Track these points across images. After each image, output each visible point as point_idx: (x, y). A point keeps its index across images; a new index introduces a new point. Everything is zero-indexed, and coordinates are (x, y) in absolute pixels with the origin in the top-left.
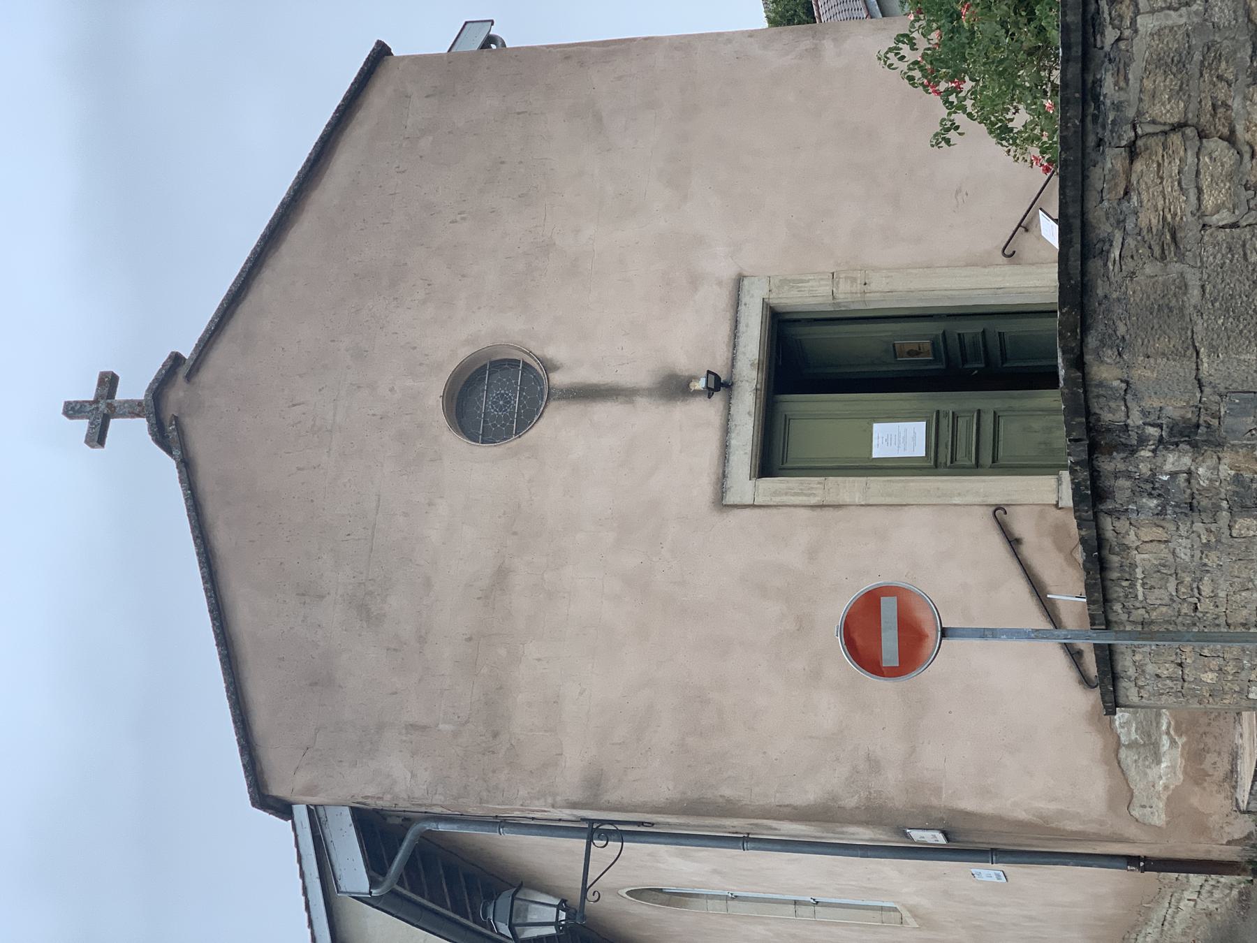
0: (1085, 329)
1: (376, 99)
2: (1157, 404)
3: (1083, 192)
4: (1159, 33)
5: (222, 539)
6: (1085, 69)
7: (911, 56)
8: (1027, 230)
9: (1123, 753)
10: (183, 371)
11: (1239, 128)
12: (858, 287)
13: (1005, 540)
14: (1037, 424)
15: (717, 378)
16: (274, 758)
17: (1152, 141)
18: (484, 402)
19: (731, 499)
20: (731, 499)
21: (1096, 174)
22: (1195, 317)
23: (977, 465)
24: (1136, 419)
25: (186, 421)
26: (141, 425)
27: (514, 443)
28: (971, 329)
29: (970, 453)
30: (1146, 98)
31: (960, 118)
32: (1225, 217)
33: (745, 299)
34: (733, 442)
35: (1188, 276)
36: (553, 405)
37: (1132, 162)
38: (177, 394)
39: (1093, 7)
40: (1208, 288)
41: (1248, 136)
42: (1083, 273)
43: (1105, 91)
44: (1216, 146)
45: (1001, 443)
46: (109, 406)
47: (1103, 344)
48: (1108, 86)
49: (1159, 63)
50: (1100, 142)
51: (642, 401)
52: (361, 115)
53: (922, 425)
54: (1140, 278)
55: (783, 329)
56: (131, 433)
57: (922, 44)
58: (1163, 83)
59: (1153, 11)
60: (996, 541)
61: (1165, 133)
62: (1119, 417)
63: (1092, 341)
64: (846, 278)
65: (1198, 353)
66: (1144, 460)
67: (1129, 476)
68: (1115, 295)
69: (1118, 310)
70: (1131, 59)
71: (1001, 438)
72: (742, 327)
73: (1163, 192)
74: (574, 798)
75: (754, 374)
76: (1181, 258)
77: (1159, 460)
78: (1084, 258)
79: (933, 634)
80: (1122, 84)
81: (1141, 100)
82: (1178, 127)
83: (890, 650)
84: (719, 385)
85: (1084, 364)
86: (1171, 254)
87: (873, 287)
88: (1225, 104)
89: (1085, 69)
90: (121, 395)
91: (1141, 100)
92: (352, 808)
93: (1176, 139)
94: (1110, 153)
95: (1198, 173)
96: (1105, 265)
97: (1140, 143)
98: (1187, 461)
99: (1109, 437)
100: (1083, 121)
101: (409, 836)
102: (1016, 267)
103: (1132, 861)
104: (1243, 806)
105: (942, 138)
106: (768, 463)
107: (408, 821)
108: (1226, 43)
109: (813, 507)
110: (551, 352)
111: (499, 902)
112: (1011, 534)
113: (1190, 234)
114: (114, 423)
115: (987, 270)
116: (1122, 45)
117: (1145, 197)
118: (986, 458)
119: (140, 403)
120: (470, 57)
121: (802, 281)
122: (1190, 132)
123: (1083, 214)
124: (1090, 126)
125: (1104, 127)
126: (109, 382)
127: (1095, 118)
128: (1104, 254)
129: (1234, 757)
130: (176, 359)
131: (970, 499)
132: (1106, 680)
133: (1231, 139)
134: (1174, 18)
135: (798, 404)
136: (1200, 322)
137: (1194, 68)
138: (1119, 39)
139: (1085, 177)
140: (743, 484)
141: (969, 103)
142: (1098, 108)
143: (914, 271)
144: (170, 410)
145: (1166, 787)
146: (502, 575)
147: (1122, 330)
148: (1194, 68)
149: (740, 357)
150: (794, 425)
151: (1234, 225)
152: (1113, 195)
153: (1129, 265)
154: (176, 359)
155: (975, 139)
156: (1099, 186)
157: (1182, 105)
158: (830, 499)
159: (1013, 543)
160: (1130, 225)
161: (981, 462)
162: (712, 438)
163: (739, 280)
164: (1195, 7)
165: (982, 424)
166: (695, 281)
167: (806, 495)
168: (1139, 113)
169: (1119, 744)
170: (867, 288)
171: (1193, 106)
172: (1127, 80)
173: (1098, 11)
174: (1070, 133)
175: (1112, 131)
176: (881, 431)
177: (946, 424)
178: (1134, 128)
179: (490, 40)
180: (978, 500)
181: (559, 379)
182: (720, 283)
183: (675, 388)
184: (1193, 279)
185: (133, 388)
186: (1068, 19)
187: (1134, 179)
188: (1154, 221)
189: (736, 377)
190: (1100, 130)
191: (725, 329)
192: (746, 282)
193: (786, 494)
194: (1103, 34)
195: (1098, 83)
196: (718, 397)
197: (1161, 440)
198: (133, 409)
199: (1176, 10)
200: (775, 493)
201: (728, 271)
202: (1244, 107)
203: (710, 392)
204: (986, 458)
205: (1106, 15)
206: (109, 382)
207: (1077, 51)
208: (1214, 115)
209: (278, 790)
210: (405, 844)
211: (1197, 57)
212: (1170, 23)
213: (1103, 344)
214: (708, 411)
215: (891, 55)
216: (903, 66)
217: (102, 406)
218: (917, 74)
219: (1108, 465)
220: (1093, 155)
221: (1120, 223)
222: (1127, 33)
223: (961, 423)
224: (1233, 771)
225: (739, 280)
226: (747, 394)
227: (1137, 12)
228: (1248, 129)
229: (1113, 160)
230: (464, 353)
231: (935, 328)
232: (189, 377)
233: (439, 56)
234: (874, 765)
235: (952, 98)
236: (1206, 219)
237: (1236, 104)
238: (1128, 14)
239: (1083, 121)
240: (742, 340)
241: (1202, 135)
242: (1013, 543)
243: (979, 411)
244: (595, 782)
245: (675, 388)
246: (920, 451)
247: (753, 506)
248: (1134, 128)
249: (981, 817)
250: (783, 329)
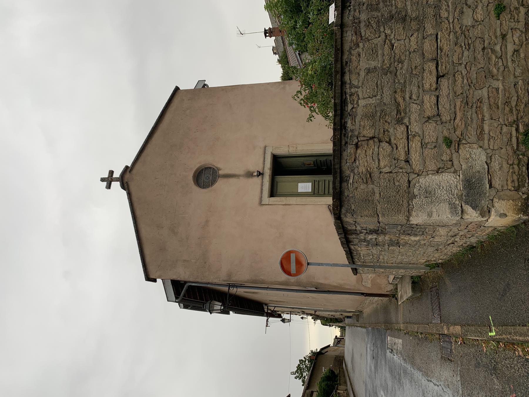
0: (341, 206)
1: (176, 101)
2: (365, 226)
3: (341, 159)
4: (366, 106)
5: (138, 213)
6: (341, 118)
7: (302, 97)
10: (129, 170)
11: (392, 139)
12: (295, 149)
15: (260, 172)
16: (150, 268)
17: (363, 143)
18: (203, 178)
19: (263, 203)
20: (263, 203)
21: (345, 154)
22: (377, 204)
23: (324, 194)
24: (359, 228)
25: (130, 183)
26: (118, 183)
27: (210, 188)
28: (323, 159)
30: (361, 128)
31: (314, 114)
32: (387, 169)
33: (266, 152)
35: (375, 189)
36: (220, 179)
37: (357, 149)
38: (127, 176)
39: (344, 97)
40: (382, 194)
41: (395, 142)
42: (341, 187)
43: (348, 125)
44: (384, 145)
46: (111, 179)
47: (347, 211)
48: (349, 124)
49: (366, 116)
50: (346, 143)
51: (241, 178)
52: (172, 105)
54: (359, 190)
55: (276, 158)
56: (116, 185)
57: (303, 93)
58: (367, 123)
59: (364, 99)
61: (367, 140)
62: (354, 228)
63: (343, 211)
65: (378, 216)
66: (362, 236)
67: (357, 238)
68: (351, 195)
69: (352, 200)
70: (357, 115)
72: (266, 159)
73: (367, 160)
74: (225, 279)
75: (269, 171)
76: (373, 184)
77: (366, 236)
78: (341, 182)
79: (305, 264)
80: (354, 123)
81: (360, 129)
82: (372, 138)
83: (293, 268)
84: (260, 174)
85: (341, 218)
86: (369, 182)
87: (298, 149)
88: (387, 130)
89: (341, 118)
90: (114, 176)
91: (360, 129)
92: (171, 280)
93: (371, 142)
94: (349, 146)
95: (378, 154)
96: (348, 185)
97: (359, 143)
98: (375, 237)
99: (350, 232)
100: (341, 136)
101: (185, 286)
103: (363, 294)
104: (391, 282)
105: (310, 119)
106: (272, 194)
107: (186, 282)
108: (388, 109)
110: (219, 166)
113: (376, 175)
114: (113, 183)
116: (354, 110)
117: (361, 162)
118: (326, 192)
119: (118, 178)
120: (200, 89)
122: (376, 140)
123: (340, 167)
124: (343, 137)
125: (347, 138)
126: (111, 173)
127: (345, 135)
128: (347, 181)
130: (127, 167)
132: (355, 271)
133: (389, 142)
134: (372, 101)
135: (280, 179)
136: (379, 205)
137: (377, 118)
138: (353, 108)
139: (341, 155)
140: (266, 199)
141: (317, 110)
142: (345, 131)
144: (126, 180)
145: (371, 277)
147: (353, 207)
148: (377, 118)
150: (279, 184)
151: (391, 172)
152: (350, 161)
153: (356, 185)
155: (319, 118)
156: (346, 158)
157: (373, 130)
160: (356, 171)
163: (265, 147)
164: (378, 97)
168: (359, 133)
171: (377, 131)
172: (355, 122)
173: (346, 98)
174: (336, 140)
175: (350, 139)
178: (358, 138)
179: (205, 85)
181: (221, 172)
183: (249, 175)
184: (377, 191)
185: (117, 175)
186: (336, 101)
187: (357, 155)
188: (364, 170)
190: (346, 139)
191: (262, 159)
192: (267, 148)
194: (347, 106)
195: (346, 123)
197: (367, 233)
198: (117, 180)
199: (371, 98)
201: (262, 145)
202: (394, 132)
203: (258, 176)
204: (326, 192)
205: (349, 100)
206: (111, 173)
207: (339, 112)
208: (384, 134)
209: (152, 276)
210: (183, 291)
211: (378, 114)
212: (369, 102)
213: (347, 211)
214: (258, 180)
215: (295, 97)
216: (299, 100)
217: (110, 179)
218: (302, 102)
219: (351, 237)
220: (344, 147)
221: (353, 171)
222: (355, 106)
225: (265, 147)
227: (359, 99)
228: (395, 139)
229: (350, 149)
230: (198, 166)
231: (314, 159)
232: (130, 172)
233: (191, 90)
235: (312, 109)
236: (381, 170)
237: (391, 130)
238: (356, 99)
239: (341, 136)
240: (266, 163)
241: (380, 141)
244: (230, 275)
245: (249, 175)
246: (310, 190)
248: (358, 138)
249: (325, 285)
250: (276, 158)
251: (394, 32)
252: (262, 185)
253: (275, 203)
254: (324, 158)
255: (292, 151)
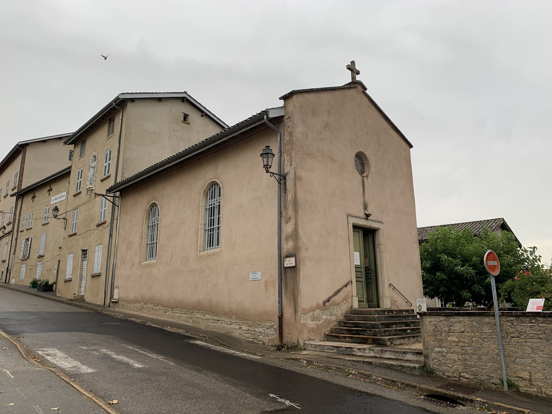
1: (404, 144)
9: (312, 312)
10: (363, 90)
14: (361, 291)
25: (355, 89)
56: (347, 78)
60: (345, 282)
111: (25, 153)
129: (313, 340)
130: (366, 89)
146: (334, 161)
154: (366, 89)
159: (346, 286)
162: (357, 215)
169: (314, 311)
183: (365, 207)
185: (358, 78)
196: (364, 216)
198: (353, 78)
203: (366, 214)
224: (311, 340)
234: (307, 250)
240: (358, 219)
242: (346, 286)
245: (365, 207)
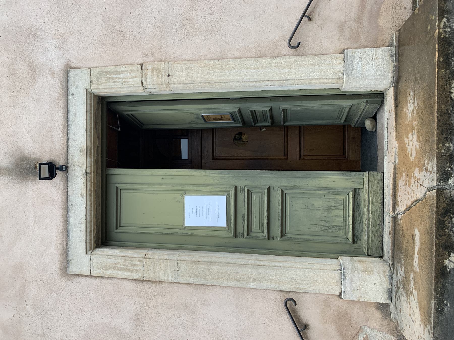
8: (310, 19)
13: (295, 330)
14: (318, 203)
19: (73, 269)
29: (262, 224)
33: (72, 90)
34: (71, 220)
45: (288, 219)
53: (223, 200)
64: (153, 69)
71: (288, 213)
72: (71, 117)
87: (176, 77)
102: (301, 58)
106: (104, 234)
109: (136, 280)
112: (299, 319)
115: (275, 61)
121: (116, 72)
131: (263, 285)
140: (81, 259)
143: (211, 62)
149: (71, 143)
150: (124, 195)
158: (149, 275)
161: (272, 234)
163: (68, 69)
165: (272, 199)
166: (34, 72)
167: (129, 271)
170: (171, 80)
176: (192, 202)
177: (242, 198)
180: (272, 286)
182: (52, 74)
189: (70, 163)
191: (60, 115)
192: (72, 73)
193: (114, 268)
200: (106, 267)
201: (58, 65)
214: (51, 189)
223: (255, 198)
226: (79, 178)
231: (234, 107)
240: (72, 128)
243: (269, 189)
247: (90, 276)
251: (207, 210)
252: (66, 209)
253: (108, 273)
254: (266, 107)
255: (155, 85)
